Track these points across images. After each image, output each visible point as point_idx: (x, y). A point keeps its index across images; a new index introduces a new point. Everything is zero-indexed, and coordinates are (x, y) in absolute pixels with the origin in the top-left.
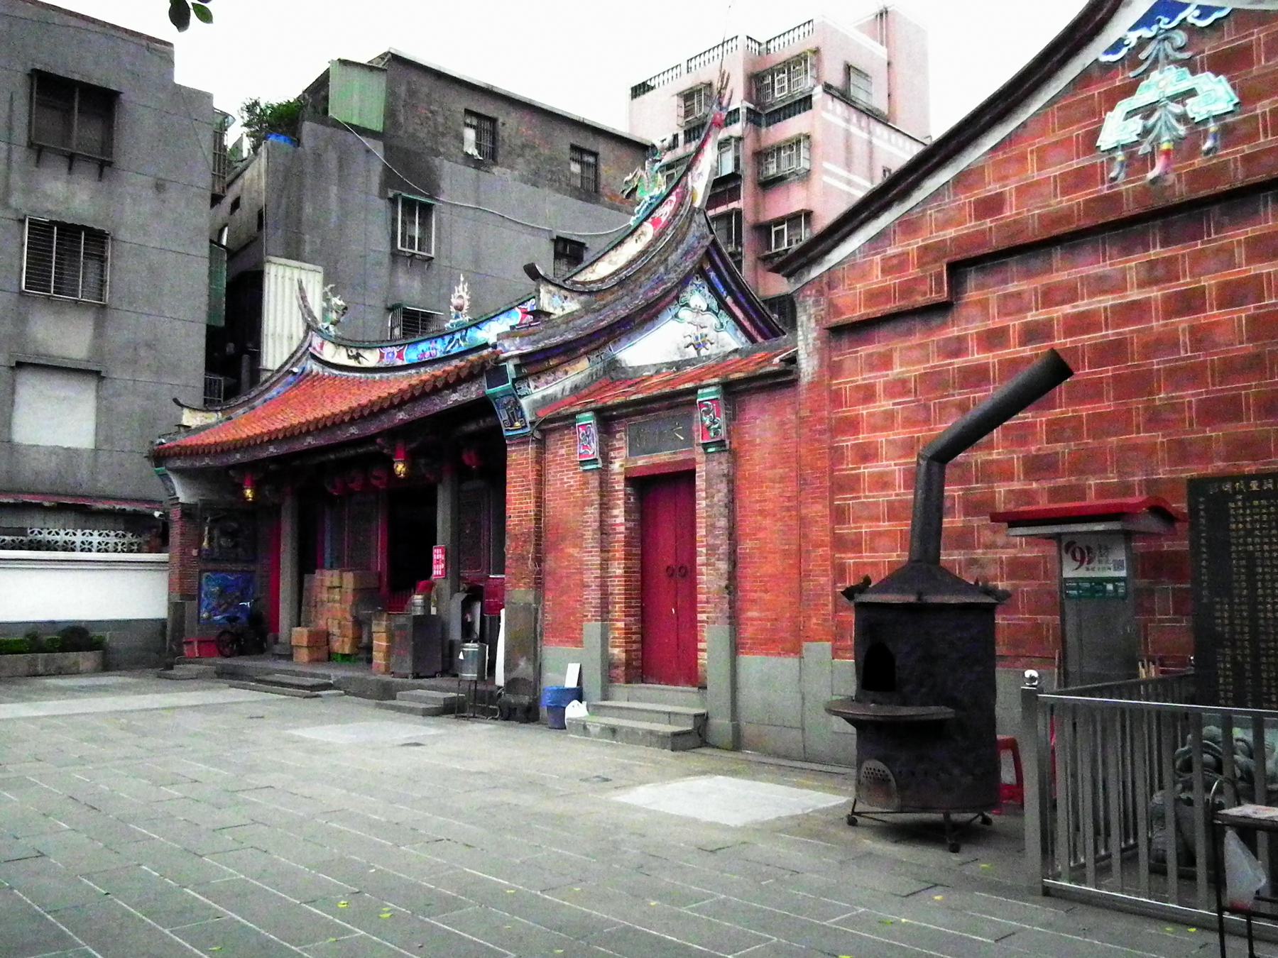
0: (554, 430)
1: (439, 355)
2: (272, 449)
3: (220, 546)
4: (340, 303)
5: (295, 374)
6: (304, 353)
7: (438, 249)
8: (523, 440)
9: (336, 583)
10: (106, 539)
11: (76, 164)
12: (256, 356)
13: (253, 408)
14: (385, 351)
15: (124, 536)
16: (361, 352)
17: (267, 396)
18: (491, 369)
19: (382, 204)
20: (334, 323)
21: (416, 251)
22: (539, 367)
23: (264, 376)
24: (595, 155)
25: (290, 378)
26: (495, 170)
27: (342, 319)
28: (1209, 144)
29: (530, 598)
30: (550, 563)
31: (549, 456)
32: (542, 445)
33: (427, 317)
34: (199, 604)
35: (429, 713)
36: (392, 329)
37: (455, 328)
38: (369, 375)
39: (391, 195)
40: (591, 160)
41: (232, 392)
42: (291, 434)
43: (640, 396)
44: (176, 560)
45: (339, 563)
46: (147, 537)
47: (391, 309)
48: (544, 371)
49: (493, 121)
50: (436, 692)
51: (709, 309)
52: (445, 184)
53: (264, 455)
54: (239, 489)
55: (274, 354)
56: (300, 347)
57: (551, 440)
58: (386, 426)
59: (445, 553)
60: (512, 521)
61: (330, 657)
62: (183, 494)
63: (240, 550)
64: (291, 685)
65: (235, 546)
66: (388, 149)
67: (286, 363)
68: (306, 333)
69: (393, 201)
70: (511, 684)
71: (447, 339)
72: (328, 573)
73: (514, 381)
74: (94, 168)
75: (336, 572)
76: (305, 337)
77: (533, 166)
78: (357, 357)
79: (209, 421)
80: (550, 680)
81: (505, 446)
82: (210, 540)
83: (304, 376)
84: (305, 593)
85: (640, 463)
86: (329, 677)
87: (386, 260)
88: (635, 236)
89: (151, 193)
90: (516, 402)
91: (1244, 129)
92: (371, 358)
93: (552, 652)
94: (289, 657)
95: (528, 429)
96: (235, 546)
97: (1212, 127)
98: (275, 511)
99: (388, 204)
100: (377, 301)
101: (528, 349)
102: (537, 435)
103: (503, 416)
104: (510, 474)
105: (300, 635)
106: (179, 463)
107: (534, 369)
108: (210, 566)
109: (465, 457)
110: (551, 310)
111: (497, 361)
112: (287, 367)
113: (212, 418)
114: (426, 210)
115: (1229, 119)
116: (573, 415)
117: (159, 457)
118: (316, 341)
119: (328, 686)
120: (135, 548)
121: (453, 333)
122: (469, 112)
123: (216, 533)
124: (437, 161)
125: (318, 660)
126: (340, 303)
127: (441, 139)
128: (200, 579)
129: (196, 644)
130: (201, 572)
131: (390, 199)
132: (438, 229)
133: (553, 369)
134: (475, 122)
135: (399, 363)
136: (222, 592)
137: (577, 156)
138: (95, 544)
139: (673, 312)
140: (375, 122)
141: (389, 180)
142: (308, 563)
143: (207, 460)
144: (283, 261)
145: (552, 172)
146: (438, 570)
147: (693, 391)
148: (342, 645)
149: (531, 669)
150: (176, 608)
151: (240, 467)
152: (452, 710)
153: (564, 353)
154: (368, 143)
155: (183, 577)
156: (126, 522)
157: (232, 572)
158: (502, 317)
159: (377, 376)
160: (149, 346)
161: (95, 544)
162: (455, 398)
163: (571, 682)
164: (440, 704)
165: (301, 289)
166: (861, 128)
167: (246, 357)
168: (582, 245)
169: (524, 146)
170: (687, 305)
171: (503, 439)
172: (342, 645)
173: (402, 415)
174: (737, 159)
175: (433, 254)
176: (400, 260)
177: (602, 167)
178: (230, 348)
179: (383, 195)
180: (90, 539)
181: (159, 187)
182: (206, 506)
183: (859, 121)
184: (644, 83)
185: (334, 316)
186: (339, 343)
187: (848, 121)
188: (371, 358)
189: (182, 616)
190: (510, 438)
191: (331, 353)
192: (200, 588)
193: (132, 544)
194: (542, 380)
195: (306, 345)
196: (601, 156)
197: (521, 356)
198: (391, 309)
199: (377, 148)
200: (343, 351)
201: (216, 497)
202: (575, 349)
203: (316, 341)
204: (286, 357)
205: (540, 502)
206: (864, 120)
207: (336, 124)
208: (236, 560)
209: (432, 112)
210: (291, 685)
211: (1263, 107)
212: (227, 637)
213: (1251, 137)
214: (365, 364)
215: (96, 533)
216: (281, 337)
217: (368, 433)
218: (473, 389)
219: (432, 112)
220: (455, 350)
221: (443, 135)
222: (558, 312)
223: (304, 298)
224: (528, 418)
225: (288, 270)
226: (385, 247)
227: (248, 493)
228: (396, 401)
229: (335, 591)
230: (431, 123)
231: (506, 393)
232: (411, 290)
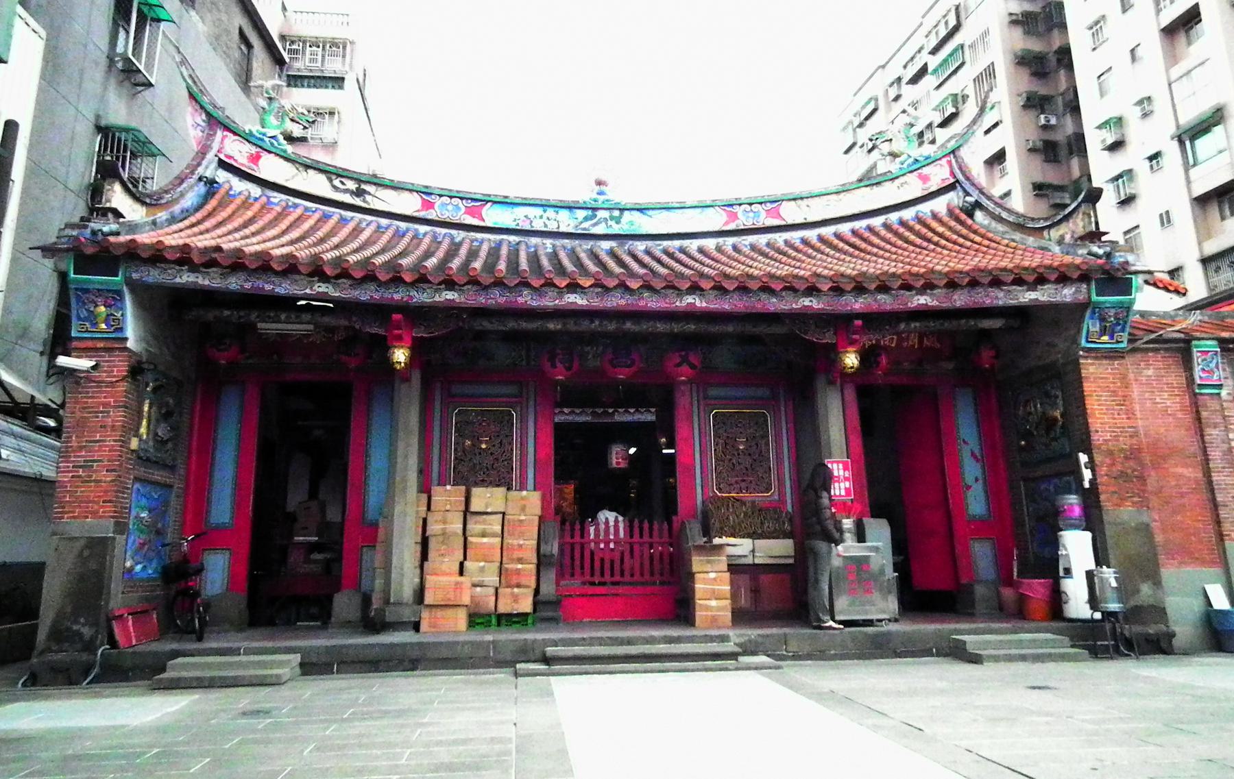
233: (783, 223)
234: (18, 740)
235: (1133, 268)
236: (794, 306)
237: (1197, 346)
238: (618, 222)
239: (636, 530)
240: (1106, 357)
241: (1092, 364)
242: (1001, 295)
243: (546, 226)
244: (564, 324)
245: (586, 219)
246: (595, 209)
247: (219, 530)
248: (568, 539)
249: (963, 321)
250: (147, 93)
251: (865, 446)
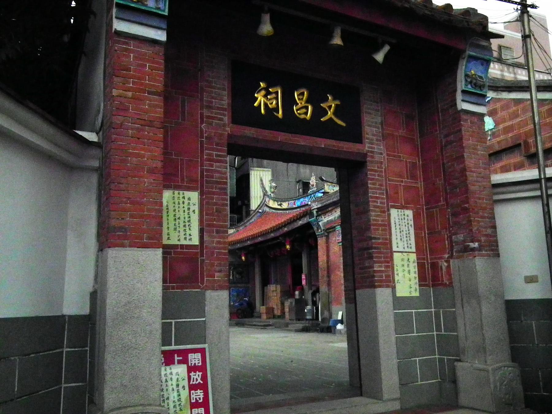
0: (330, 232)
2: (260, 238)
3: (236, 277)
4: (274, 185)
8: (322, 236)
9: (275, 289)
12: (248, 205)
14: (290, 202)
17: (251, 221)
20: (273, 193)
22: (325, 211)
23: (251, 212)
25: (259, 214)
28: (489, 138)
29: (327, 290)
30: (332, 277)
31: (330, 241)
32: (327, 237)
35: (298, 331)
36: (299, 189)
38: (285, 211)
41: (240, 220)
42: (254, 237)
45: (276, 282)
47: (298, 182)
48: (327, 212)
50: (300, 325)
53: (246, 244)
54: (241, 258)
55: (254, 204)
56: (262, 202)
57: (330, 235)
59: (306, 277)
60: (320, 264)
61: (274, 317)
64: (258, 326)
68: (264, 197)
70: (323, 320)
71: (309, 197)
72: (272, 286)
73: (316, 216)
75: (274, 285)
76: (263, 198)
78: (280, 205)
80: (334, 317)
82: (233, 276)
83: (264, 212)
84: (265, 294)
90: (318, 223)
91: (497, 133)
92: (285, 205)
93: (334, 308)
94: (260, 317)
97: (489, 133)
98: (253, 264)
100: (293, 180)
101: (320, 206)
102: (326, 234)
103: (315, 229)
104: (319, 247)
105: (263, 309)
107: (323, 212)
108: (233, 285)
109: (310, 241)
110: (329, 191)
111: (311, 210)
115: (494, 130)
116: (335, 227)
118: (267, 199)
119: (270, 325)
121: (311, 195)
125: (270, 318)
126: (274, 185)
133: (331, 211)
135: (294, 206)
136: (238, 295)
142: (265, 282)
143: (249, 242)
144: (257, 169)
146: (304, 282)
147: (335, 227)
148: (277, 312)
149: (328, 315)
151: (240, 249)
152: (305, 330)
153: (334, 205)
157: (241, 287)
159: (287, 212)
162: (301, 223)
163: (340, 318)
164: (301, 328)
165: (261, 180)
166: (510, 73)
167: (244, 207)
171: (316, 235)
172: (277, 312)
173: (286, 229)
178: (240, 203)
183: (508, 69)
185: (272, 190)
186: (275, 200)
187: (502, 71)
188: (285, 205)
191: (273, 204)
197: (317, 208)
198: (298, 182)
201: (234, 260)
203: (267, 199)
204: (256, 207)
205: (328, 256)
206: (511, 69)
208: (242, 283)
210: (258, 326)
211: (501, 127)
212: (239, 311)
213: (499, 136)
216: (257, 197)
222: (332, 191)
223: (262, 184)
224: (322, 228)
225: (258, 172)
227: (243, 258)
228: (283, 225)
229: (274, 291)
231: (315, 221)
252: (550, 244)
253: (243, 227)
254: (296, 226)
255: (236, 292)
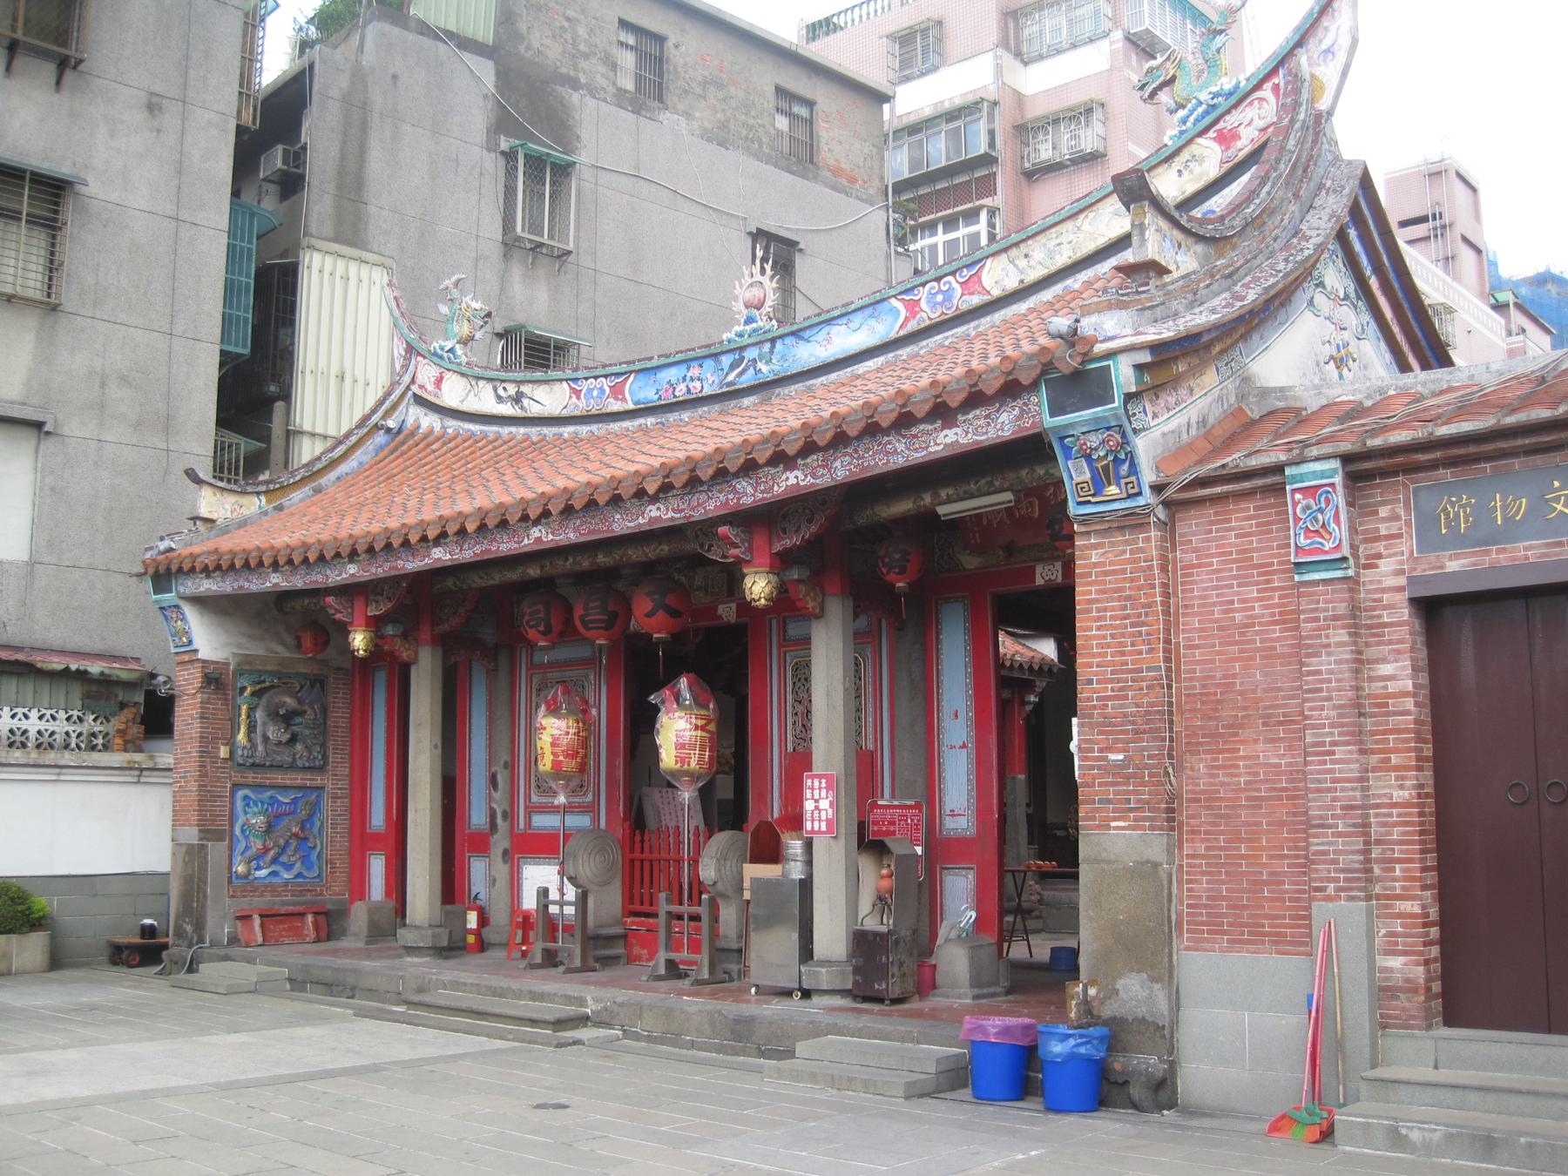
1: (707, 391)
3: (266, 739)
5: (389, 430)
6: (404, 394)
7: (577, 238)
10: (51, 726)
11: (19, 62)
13: (318, 491)
14: (584, 386)
15: (80, 719)
16: (526, 389)
18: (1075, 377)
19: (493, 165)
21: (545, 239)
24: (810, 104)
26: (666, 117)
27: (478, 335)
33: (562, 348)
34: (231, 849)
37: (746, 340)
39: (504, 144)
40: (803, 111)
41: (255, 464)
43: (1466, 427)
44: (192, 767)
46: (116, 724)
49: (660, 39)
51: (1346, 297)
52: (586, 133)
58: (747, 501)
62: (208, 641)
63: (299, 747)
65: (293, 740)
66: (503, 76)
67: (374, 411)
69: (510, 156)
71: (726, 360)
74: (50, 69)
76: (405, 367)
77: (720, 116)
78: (517, 399)
79: (246, 512)
81: (1071, 537)
82: (251, 729)
85: (1452, 566)
86: (582, 1002)
87: (493, 249)
88: (1178, 162)
89: (138, 116)
90: (1125, 441)
95: (1141, 501)
96: (293, 740)
99: (501, 162)
102: (1161, 513)
103: (1074, 474)
106: (207, 586)
108: (250, 777)
112: (375, 419)
113: (252, 505)
114: (562, 171)
116: (1278, 469)
117: (162, 576)
120: (100, 741)
122: (624, 24)
123: (259, 715)
124: (575, 98)
127: (583, 64)
128: (233, 803)
129: (257, 921)
130: (236, 786)
131: (503, 153)
132: (578, 210)
134: (631, 41)
135: (616, 406)
137: (785, 106)
138: (32, 734)
139: (1307, 296)
140: (482, 27)
141: (503, 123)
144: (336, 247)
145: (750, 128)
150: (192, 858)
154: (471, 60)
155: (206, 797)
156: (86, 696)
157: (285, 788)
158: (858, 318)
160: (125, 380)
161: (32, 734)
168: (792, 244)
169: (705, 83)
170: (1321, 284)
174: (992, 133)
175: (571, 246)
176: (517, 254)
177: (821, 127)
179: (491, 146)
180: (24, 724)
181: (153, 107)
182: (246, 666)
184: (828, 20)
189: (203, 869)
190: (1086, 520)
192: (232, 819)
193: (94, 735)
194: (1161, 401)
195: (407, 379)
196: (817, 108)
197: (1154, 347)
199: (486, 71)
200: (486, 389)
202: (1208, 346)
203: (426, 373)
204: (371, 403)
207: (425, 29)
209: (568, 19)
214: (534, 410)
215: (34, 714)
217: (698, 515)
218: (1004, 417)
219: (568, 19)
220: (748, 379)
221: (586, 56)
224: (1148, 476)
226: (494, 229)
230: (568, 36)
232: (537, 305)
233: (987, 298)
234: (922, 1096)
235: (1099, 348)
236: (641, 521)
237: (1294, 479)
238: (769, 362)
239: (638, 846)
240: (1121, 528)
241: (1095, 547)
242: (900, 447)
243: (689, 391)
244: (542, 568)
245: (732, 367)
246: (742, 349)
247: (376, 837)
248: (637, 855)
249: (1024, 473)
250: (571, 258)
251: (1429, 654)
252: (477, 581)
253: (307, 489)
254: (899, 461)
255: (264, 812)
